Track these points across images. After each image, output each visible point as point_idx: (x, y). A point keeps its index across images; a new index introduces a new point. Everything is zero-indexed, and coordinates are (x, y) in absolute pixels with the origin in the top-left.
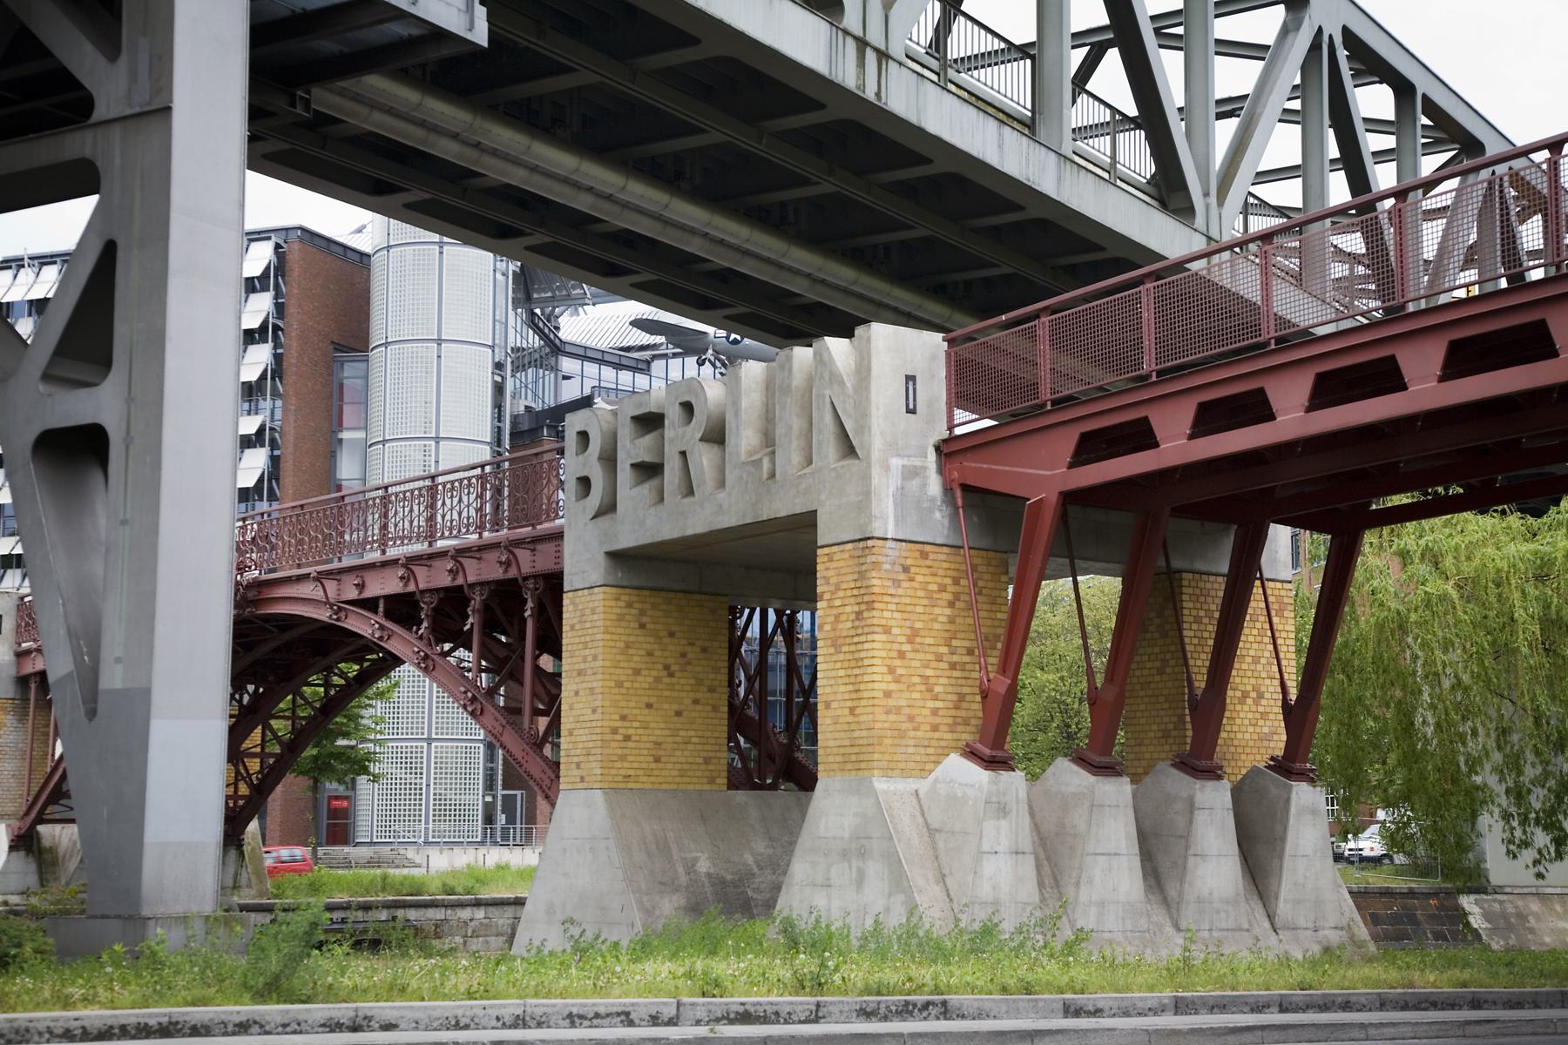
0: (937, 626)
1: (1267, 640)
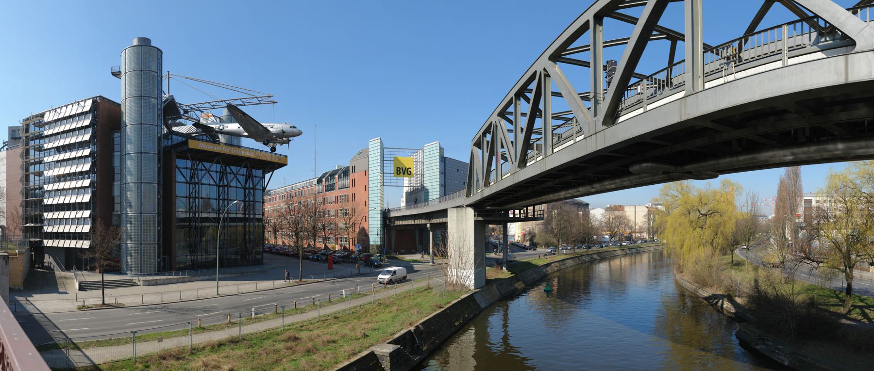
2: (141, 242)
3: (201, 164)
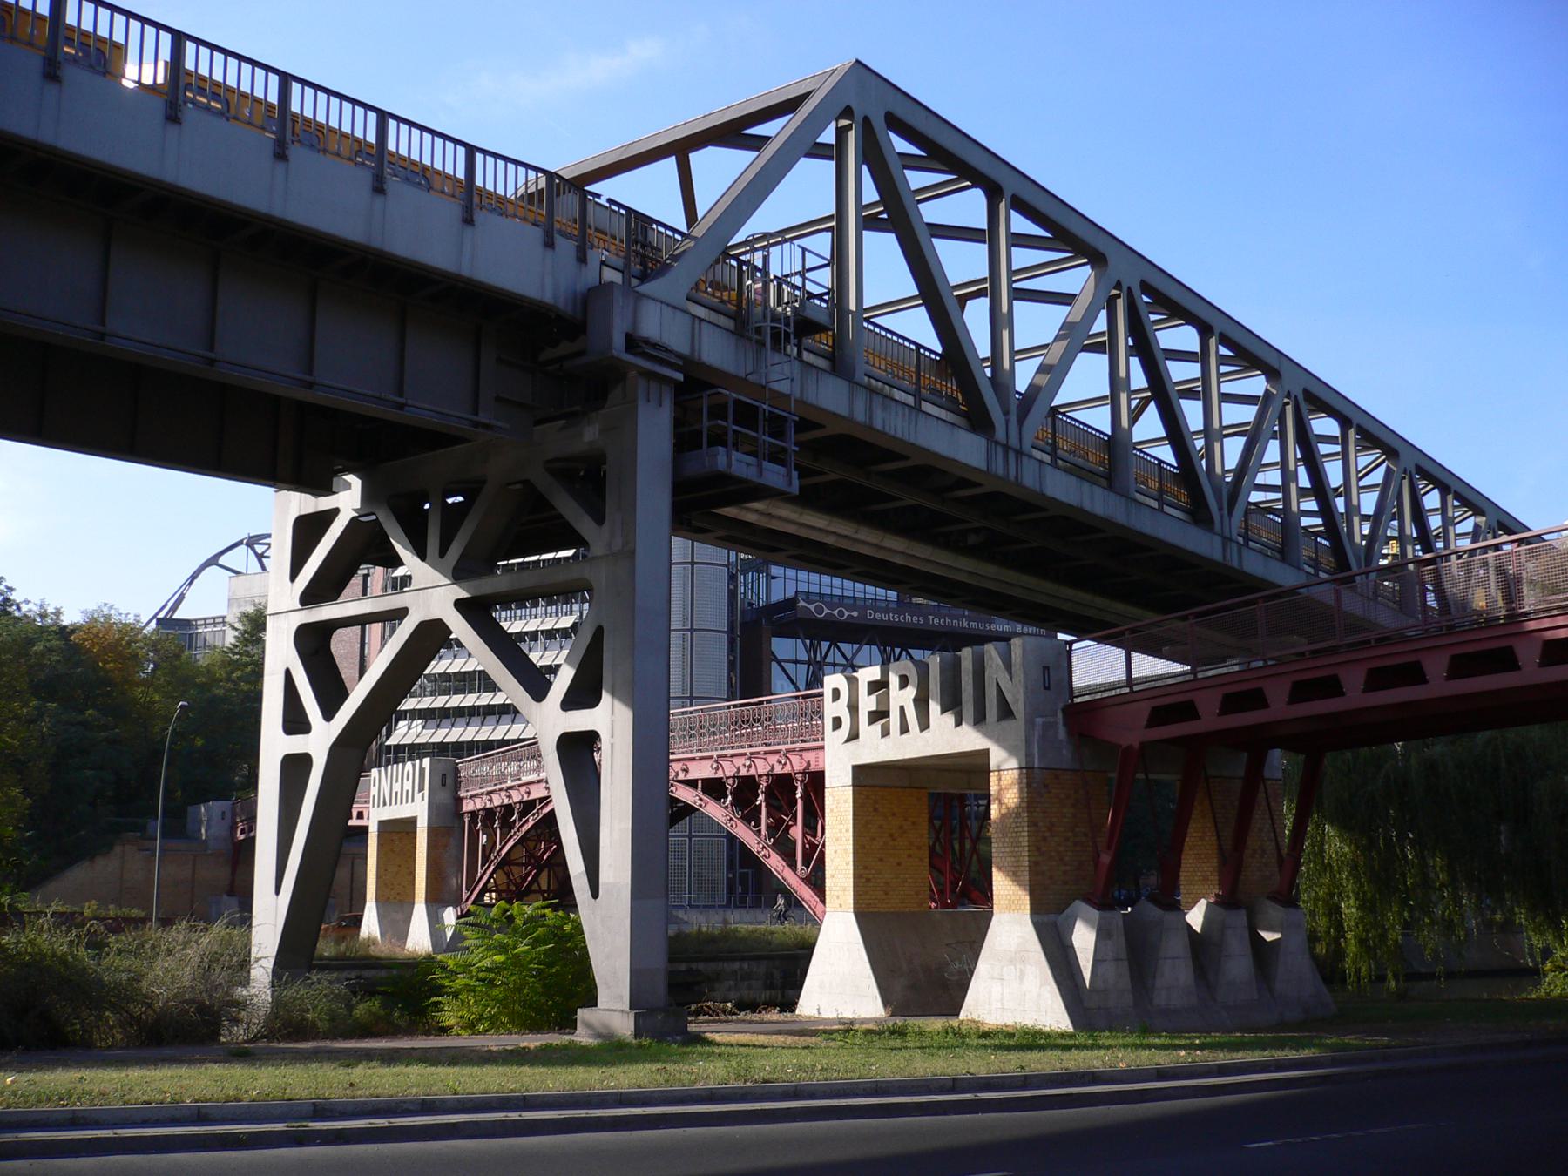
0: (1066, 820)
1: (1267, 816)
2: (694, 836)
3: (904, 653)
